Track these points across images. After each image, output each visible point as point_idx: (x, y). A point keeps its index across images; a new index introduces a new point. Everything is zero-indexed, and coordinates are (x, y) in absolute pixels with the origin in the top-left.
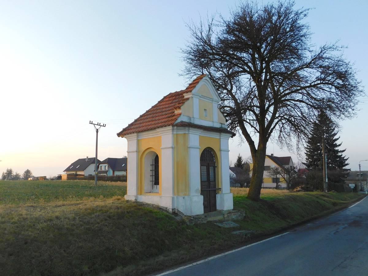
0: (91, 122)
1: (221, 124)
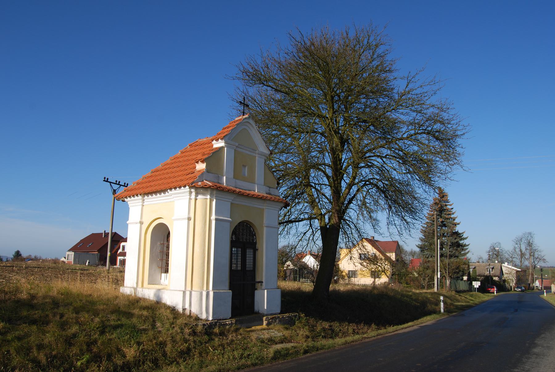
0: (106, 180)
1: (268, 188)
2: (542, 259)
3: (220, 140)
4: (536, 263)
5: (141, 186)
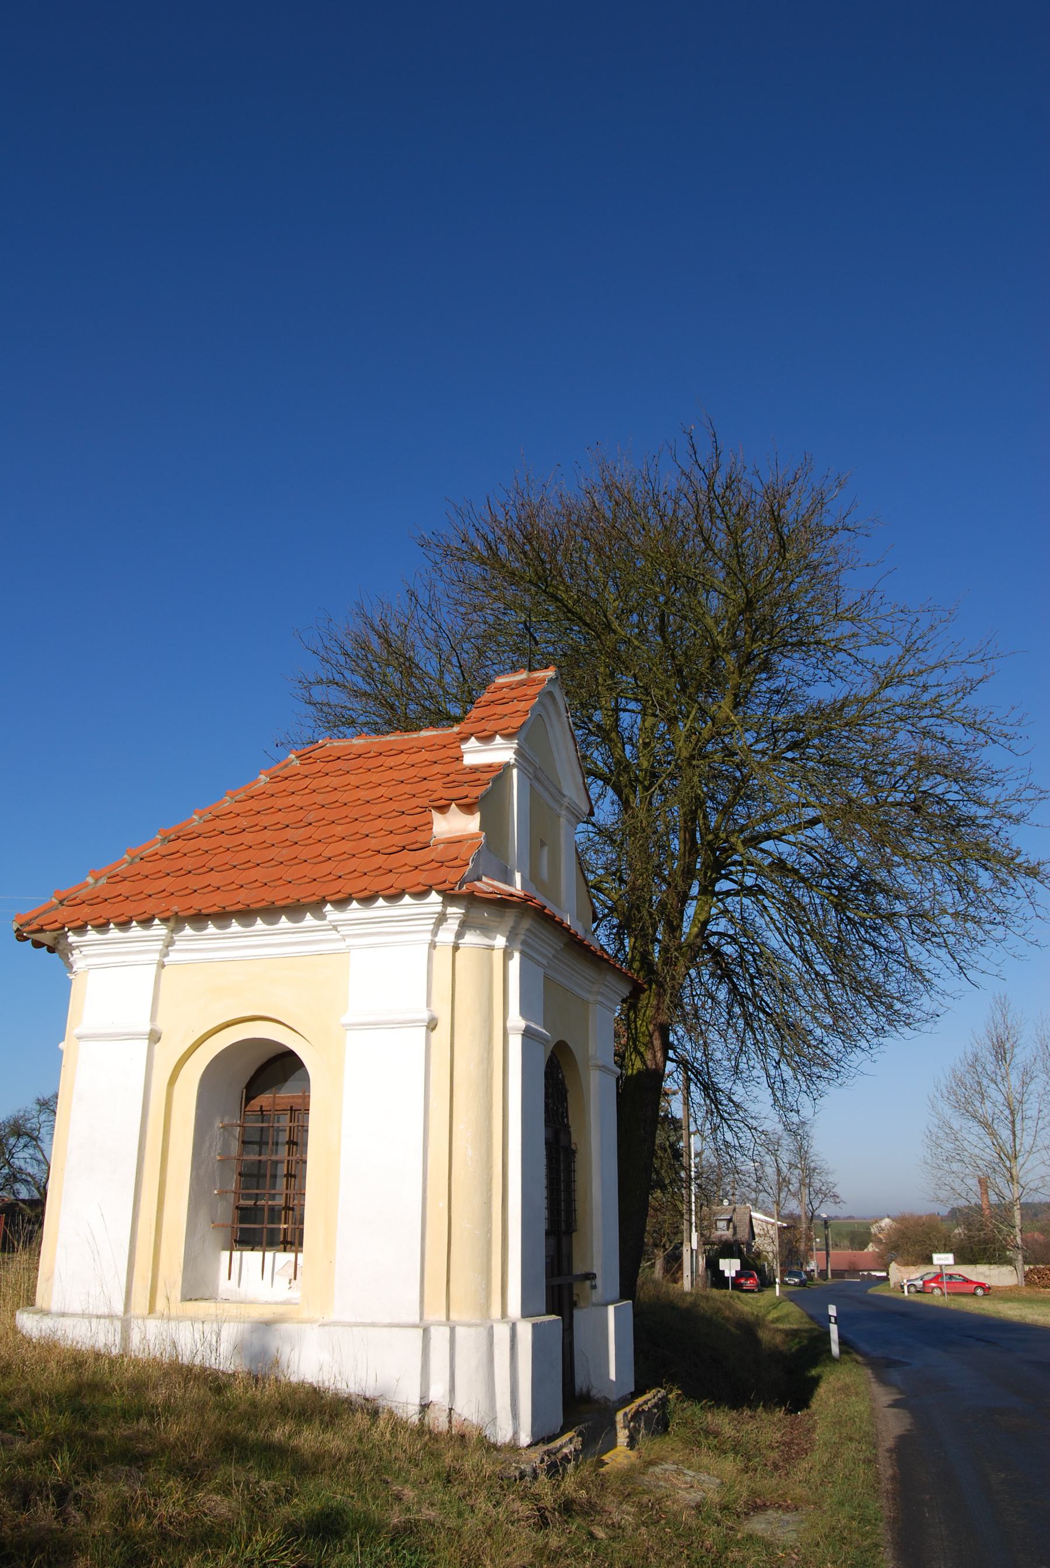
2: (831, 1194)
3: (498, 739)
4: (816, 1204)
5: (124, 888)
